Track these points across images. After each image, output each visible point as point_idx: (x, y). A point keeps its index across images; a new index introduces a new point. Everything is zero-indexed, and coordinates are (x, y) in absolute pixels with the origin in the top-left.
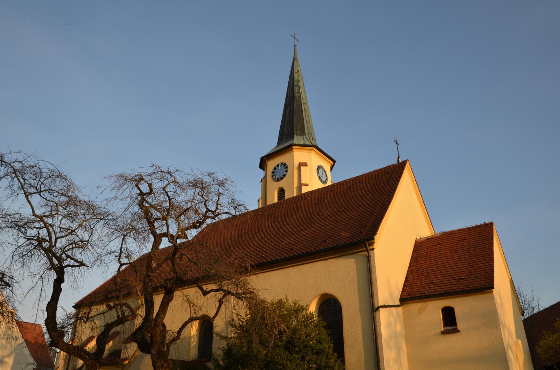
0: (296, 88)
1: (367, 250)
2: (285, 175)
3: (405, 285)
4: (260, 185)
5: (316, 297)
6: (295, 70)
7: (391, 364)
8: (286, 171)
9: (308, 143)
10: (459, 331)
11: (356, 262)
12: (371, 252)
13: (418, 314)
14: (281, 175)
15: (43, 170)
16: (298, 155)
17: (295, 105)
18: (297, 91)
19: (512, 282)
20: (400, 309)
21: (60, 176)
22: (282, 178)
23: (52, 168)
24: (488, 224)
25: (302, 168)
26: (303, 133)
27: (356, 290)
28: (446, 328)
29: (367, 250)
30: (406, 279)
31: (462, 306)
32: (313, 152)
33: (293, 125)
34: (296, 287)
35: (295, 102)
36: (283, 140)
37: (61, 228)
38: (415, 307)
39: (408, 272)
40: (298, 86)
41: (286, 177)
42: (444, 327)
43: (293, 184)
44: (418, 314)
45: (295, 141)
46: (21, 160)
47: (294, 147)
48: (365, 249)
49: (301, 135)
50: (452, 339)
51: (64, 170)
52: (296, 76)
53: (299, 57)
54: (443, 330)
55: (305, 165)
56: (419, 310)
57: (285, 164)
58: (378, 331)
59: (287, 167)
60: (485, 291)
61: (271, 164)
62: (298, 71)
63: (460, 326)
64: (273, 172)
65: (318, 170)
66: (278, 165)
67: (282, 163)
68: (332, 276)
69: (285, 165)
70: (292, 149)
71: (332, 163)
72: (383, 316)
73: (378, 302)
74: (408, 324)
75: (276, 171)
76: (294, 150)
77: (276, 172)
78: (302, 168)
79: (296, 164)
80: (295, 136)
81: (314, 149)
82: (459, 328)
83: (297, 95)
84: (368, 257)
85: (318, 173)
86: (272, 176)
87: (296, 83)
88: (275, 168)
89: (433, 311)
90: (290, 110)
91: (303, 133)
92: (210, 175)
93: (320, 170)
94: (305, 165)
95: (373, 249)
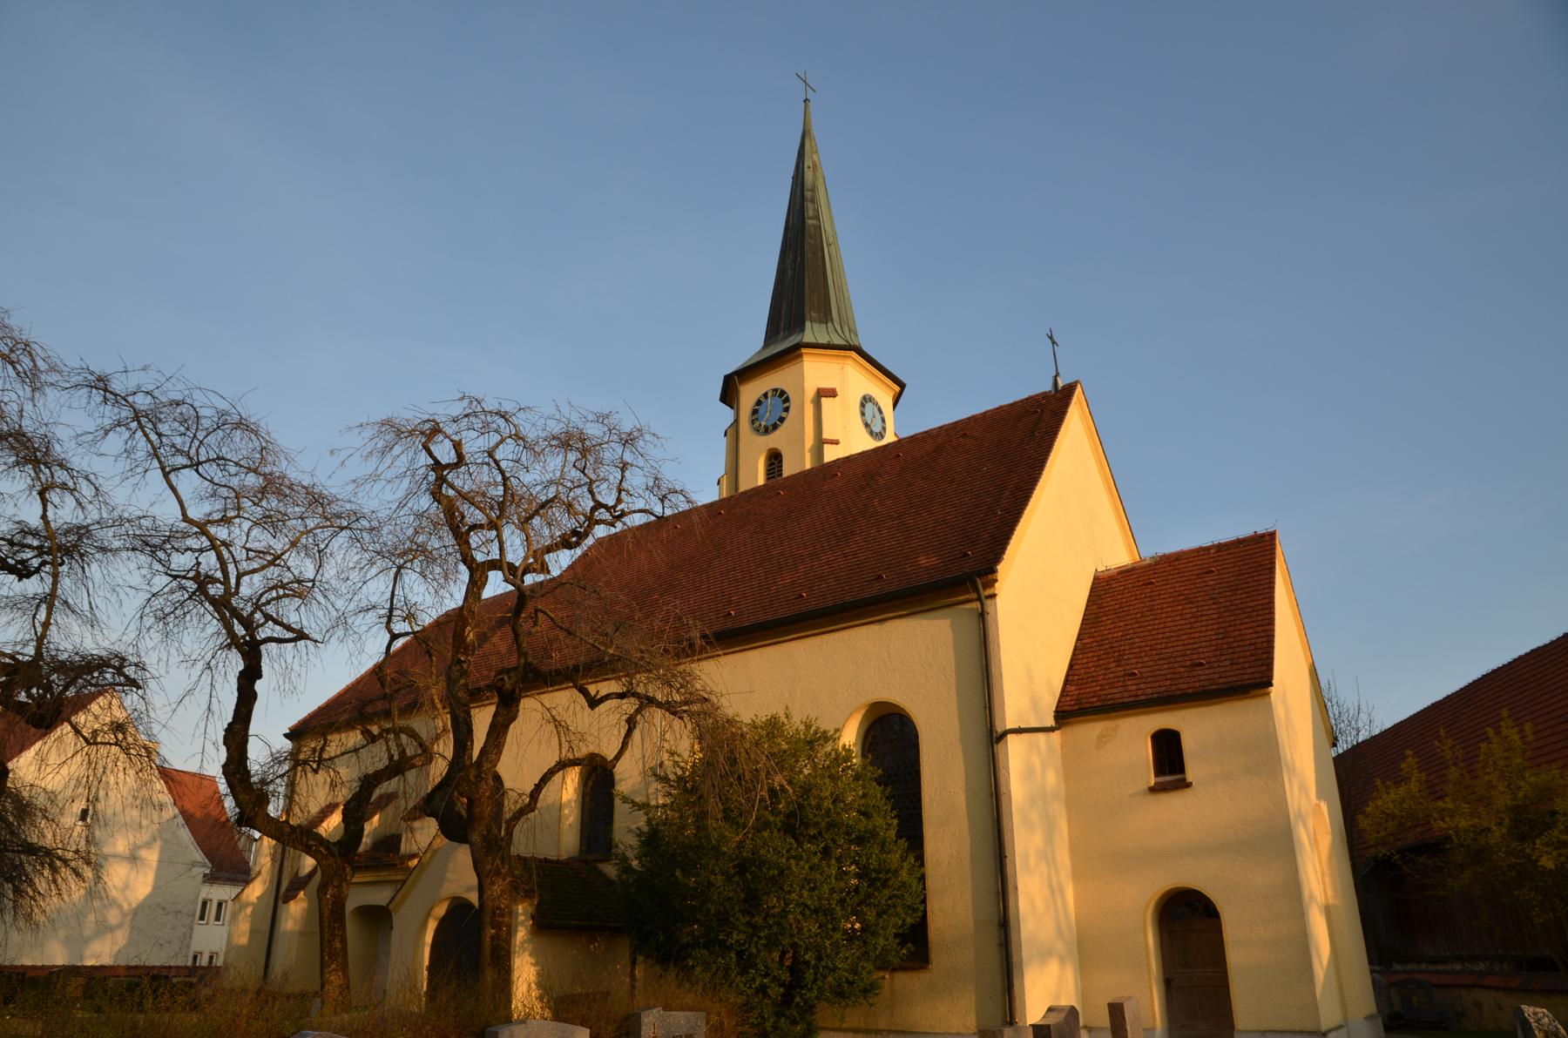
0: (810, 205)
1: (979, 599)
2: (782, 420)
3: (1067, 681)
4: (722, 444)
5: (857, 710)
7: (1032, 861)
8: (787, 410)
9: (837, 341)
10: (1189, 785)
11: (952, 626)
12: (988, 602)
13: (1098, 748)
14: (775, 420)
15: (202, 412)
16: (815, 371)
17: (807, 247)
18: (811, 213)
20: (1057, 733)
21: (242, 425)
22: (775, 427)
23: (223, 405)
24: (1263, 536)
25: (824, 400)
26: (826, 317)
27: (953, 692)
28: (1161, 779)
29: (979, 599)
30: (1071, 666)
31: (1196, 727)
32: (850, 362)
33: (802, 297)
34: (810, 687)
35: (808, 240)
36: (778, 332)
37: (248, 550)
38: (1089, 731)
39: (1075, 649)
40: (813, 201)
42: (1157, 775)
43: (803, 441)
44: (1098, 748)
45: (808, 337)
46: (150, 387)
47: (804, 350)
48: (974, 596)
49: (821, 322)
50: (1174, 802)
51: (252, 409)
52: (809, 176)
53: (816, 131)
54: (1152, 783)
55: (832, 393)
56: (1100, 737)
57: (783, 393)
58: (1003, 789)
59: (787, 400)
61: (750, 393)
62: (815, 165)
63: (1191, 774)
64: (755, 412)
65: (863, 405)
66: (766, 395)
68: (898, 659)
69: (782, 394)
70: (801, 355)
71: (898, 389)
73: (1004, 720)
74: (1071, 769)
75: (761, 409)
78: (824, 400)
79: (810, 393)
80: (808, 324)
81: (854, 354)
83: (810, 222)
85: (863, 414)
86: (753, 422)
87: (808, 194)
88: (759, 403)
89: (1132, 737)
90: (795, 261)
91: (826, 317)
92: (602, 418)
93: (869, 406)
94: (832, 393)
95: (993, 596)
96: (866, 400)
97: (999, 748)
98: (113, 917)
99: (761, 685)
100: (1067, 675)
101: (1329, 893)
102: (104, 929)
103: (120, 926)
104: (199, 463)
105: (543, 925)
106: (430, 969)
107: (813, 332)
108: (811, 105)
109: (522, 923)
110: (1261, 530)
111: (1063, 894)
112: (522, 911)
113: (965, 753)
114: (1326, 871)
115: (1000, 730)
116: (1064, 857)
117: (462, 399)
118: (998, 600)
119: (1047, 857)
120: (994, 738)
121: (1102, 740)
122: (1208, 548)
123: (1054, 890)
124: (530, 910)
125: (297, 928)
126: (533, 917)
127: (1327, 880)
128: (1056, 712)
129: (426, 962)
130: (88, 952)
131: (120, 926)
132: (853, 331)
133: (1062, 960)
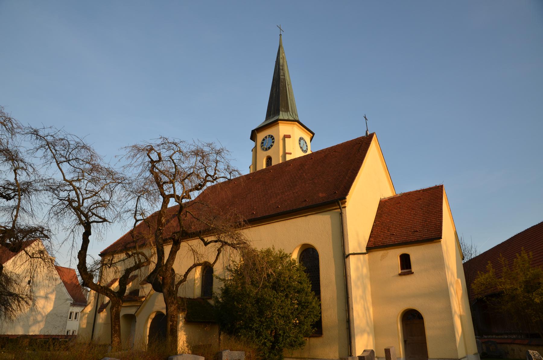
0: (282, 71)
1: (340, 208)
2: (272, 146)
3: (370, 237)
4: (251, 154)
5: (297, 247)
6: (281, 56)
7: (358, 299)
8: (273, 142)
10: (413, 273)
11: (331, 217)
12: (343, 209)
13: (381, 260)
14: (269, 146)
15: (71, 143)
16: (283, 129)
17: (281, 86)
18: (282, 74)
19: (456, 234)
20: (367, 256)
21: (84, 147)
22: (269, 148)
23: (78, 140)
24: (439, 186)
25: (286, 139)
26: (287, 110)
27: (331, 241)
28: (403, 271)
29: (340, 208)
30: (372, 231)
32: (295, 126)
33: (279, 103)
34: (281, 239)
36: (270, 116)
37: (86, 190)
38: (378, 254)
39: (373, 226)
40: (283, 70)
41: (273, 147)
42: (401, 270)
43: (279, 153)
44: (381, 260)
45: (281, 117)
48: (338, 207)
50: (408, 278)
52: (281, 61)
53: (283, 45)
54: (400, 272)
55: (289, 137)
57: (272, 136)
58: (348, 274)
59: (273, 139)
60: (435, 241)
61: (260, 136)
63: (413, 269)
64: (262, 143)
65: (300, 141)
66: (266, 137)
67: (269, 135)
68: (311, 229)
70: (278, 123)
71: (312, 135)
72: (353, 261)
74: (372, 267)
75: (265, 142)
76: (280, 124)
77: (265, 143)
78: (286, 139)
79: (281, 136)
80: (281, 112)
81: (297, 123)
82: (413, 271)
84: (341, 215)
85: (300, 144)
86: (262, 146)
87: (281, 67)
88: (264, 140)
89: (393, 257)
92: (209, 145)
93: (302, 141)
94: (289, 137)
95: (345, 207)
96: (301, 139)
97: (347, 260)
98: (39, 318)
99: (264, 238)
100: (371, 235)
101: (461, 310)
102: (36, 322)
103: (42, 321)
104: (69, 160)
105: (188, 321)
106: (149, 336)
107: (282, 115)
108: (282, 36)
109: (181, 320)
110: (438, 184)
111: (369, 311)
112: (181, 316)
113: (335, 261)
114: (460, 303)
115: (347, 254)
116: (369, 298)
117: (161, 138)
118: (347, 208)
119: (363, 298)
120: (345, 256)
121: (383, 257)
122: (419, 191)
123: (366, 309)
124: (184, 316)
125: (103, 322)
126: (185, 318)
127: (461, 306)
128: (367, 247)
129: (148, 334)
130: (30, 330)
131: (42, 321)
132: (296, 115)
133: (368, 334)
